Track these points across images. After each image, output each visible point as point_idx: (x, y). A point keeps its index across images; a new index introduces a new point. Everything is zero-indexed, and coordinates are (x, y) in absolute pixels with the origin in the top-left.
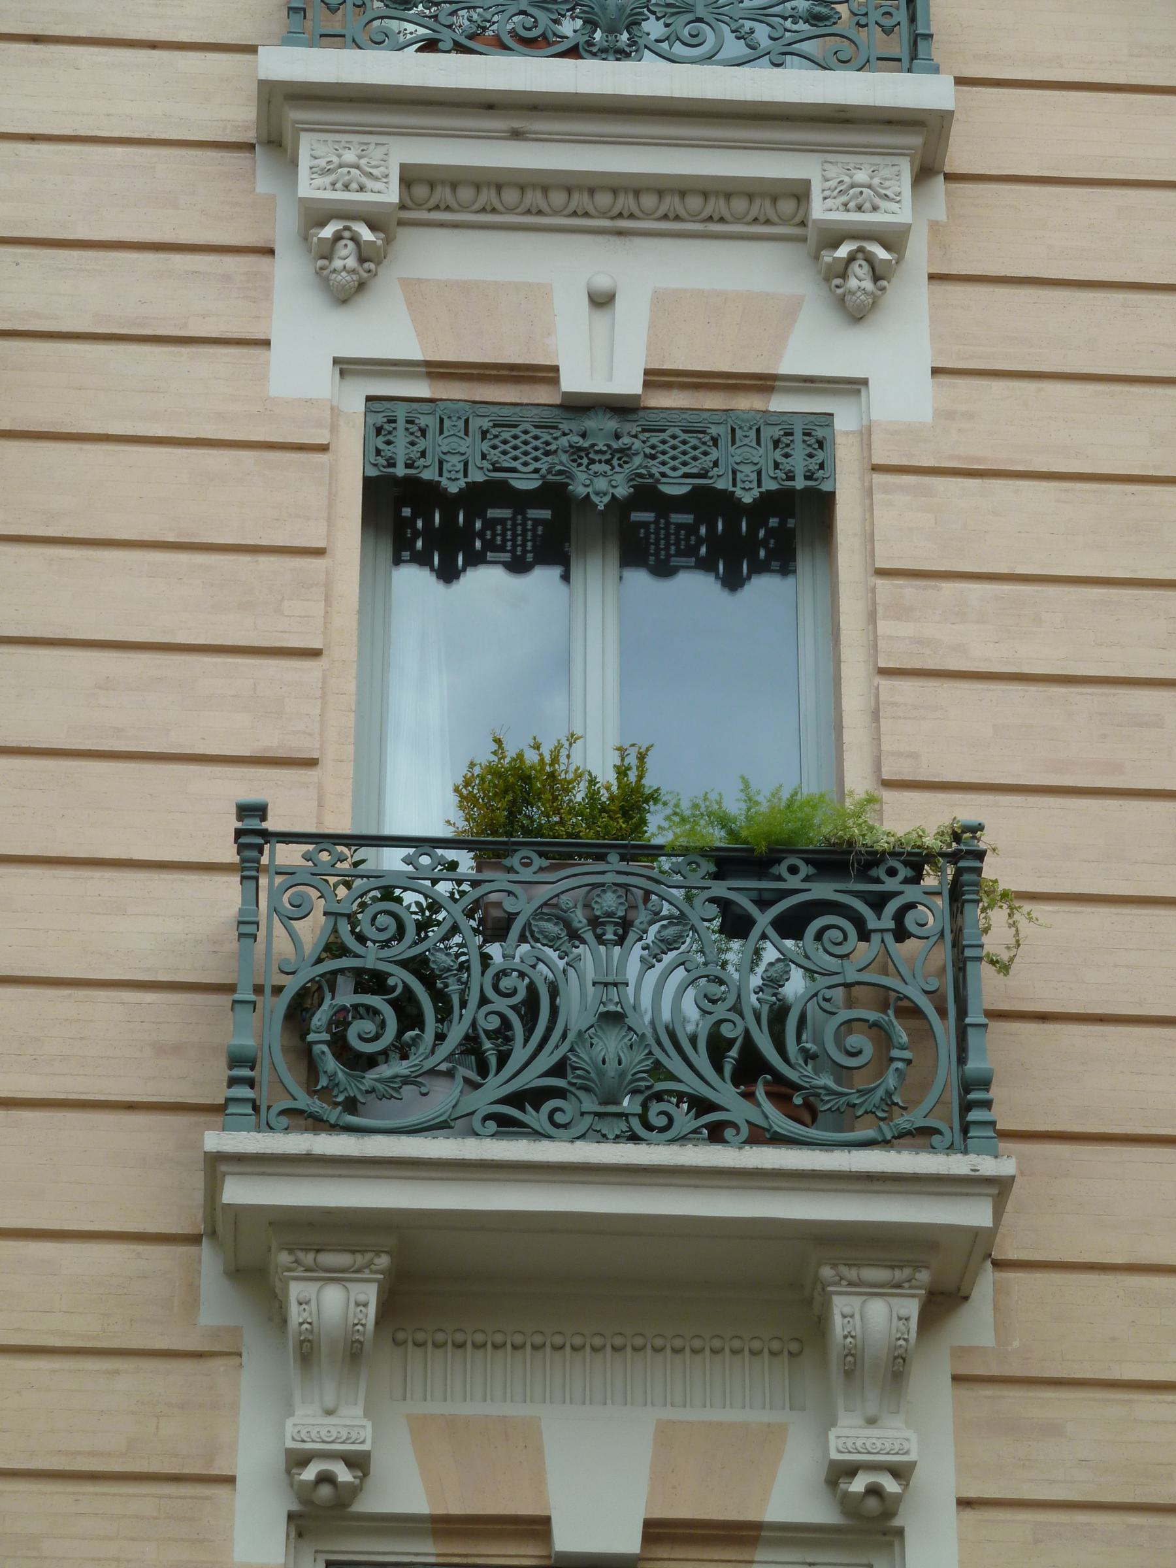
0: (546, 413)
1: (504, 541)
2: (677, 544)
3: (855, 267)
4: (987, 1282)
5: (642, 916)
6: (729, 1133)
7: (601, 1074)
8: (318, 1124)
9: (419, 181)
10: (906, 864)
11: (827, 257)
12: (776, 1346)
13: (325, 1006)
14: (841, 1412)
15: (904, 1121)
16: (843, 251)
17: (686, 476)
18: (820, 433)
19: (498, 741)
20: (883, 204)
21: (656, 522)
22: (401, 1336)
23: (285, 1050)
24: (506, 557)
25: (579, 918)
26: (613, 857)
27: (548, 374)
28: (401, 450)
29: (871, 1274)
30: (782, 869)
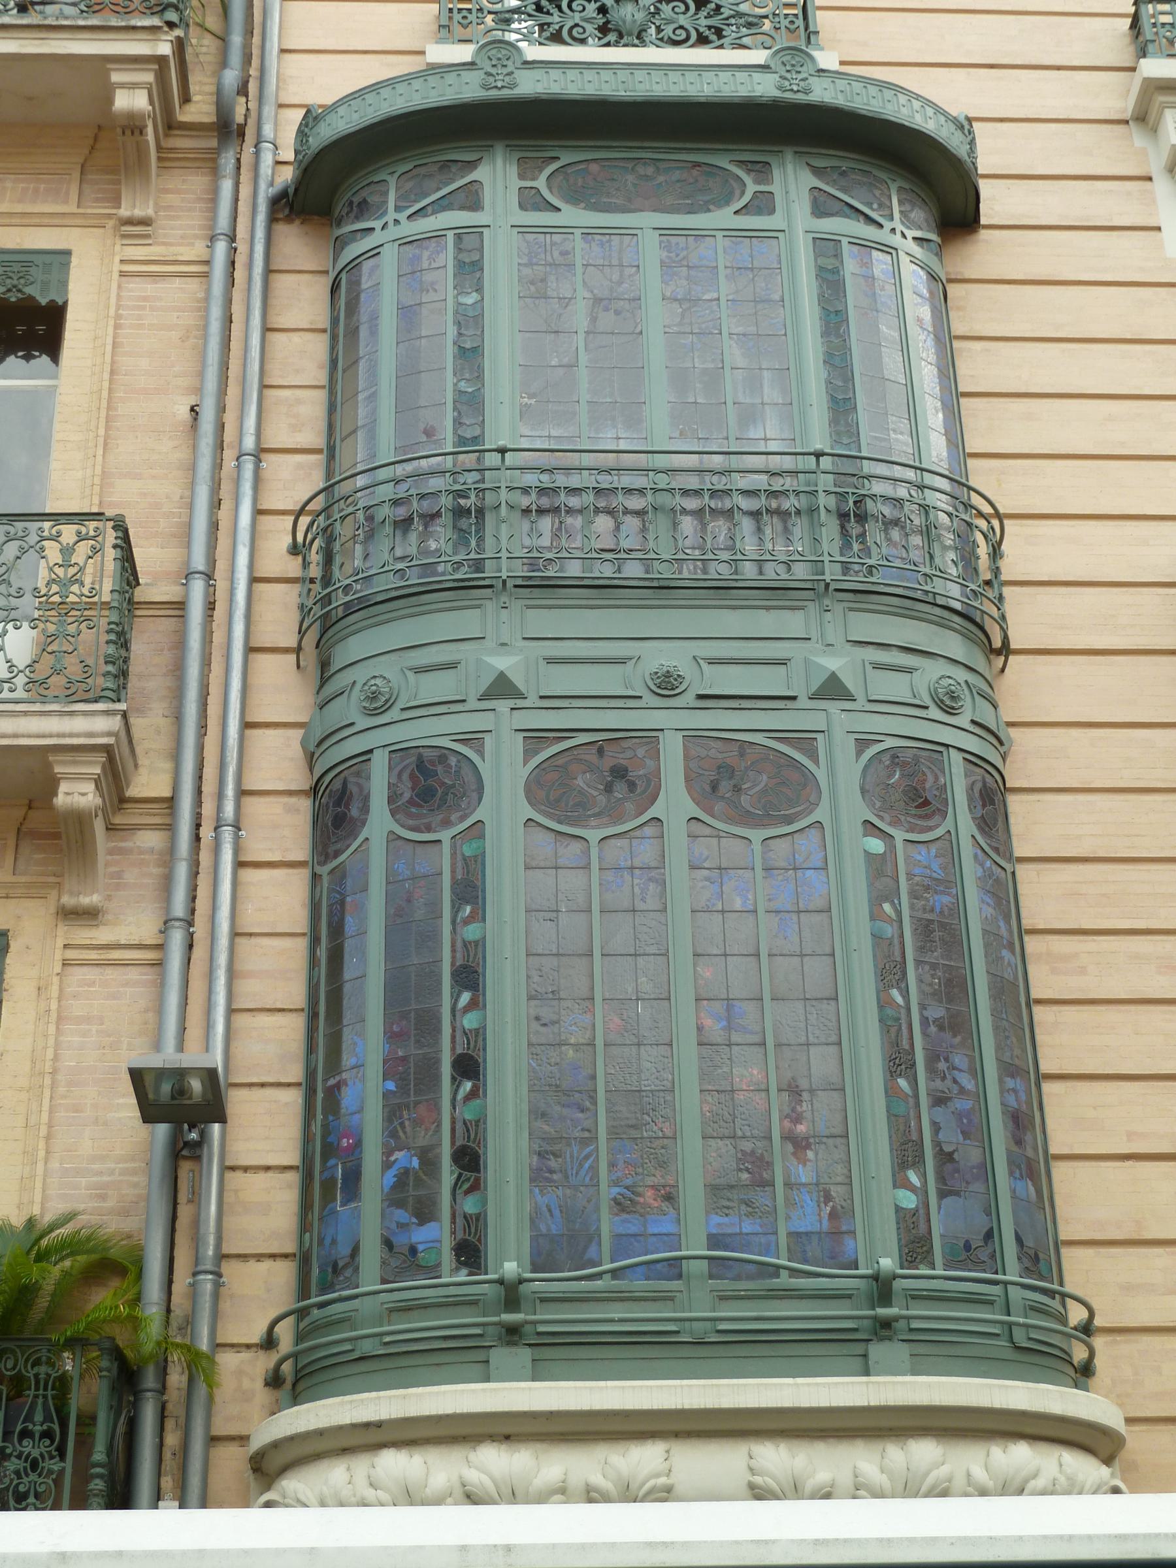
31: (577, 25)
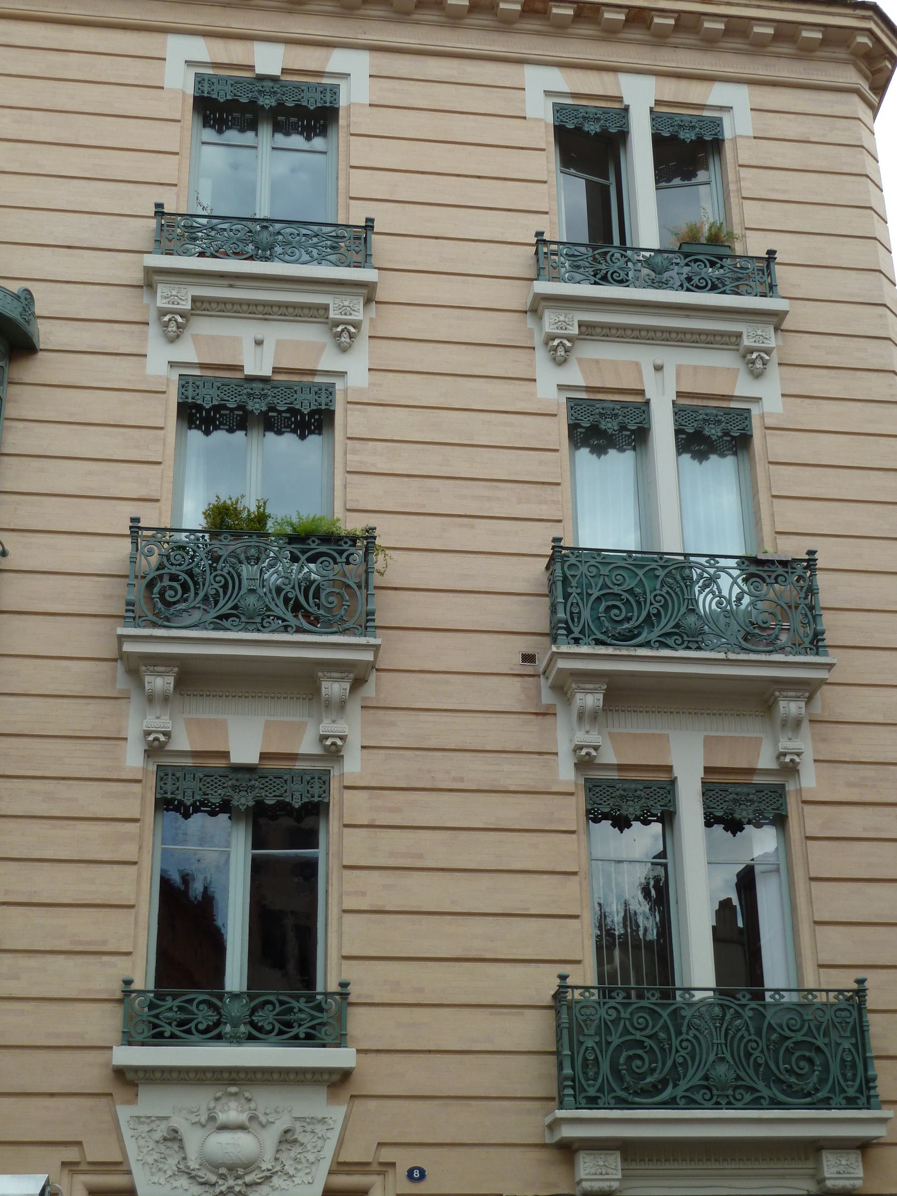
0: (239, 381)
1: (227, 422)
2: (284, 424)
3: (344, 333)
4: (373, 676)
5: (263, 557)
6: (289, 629)
7: (248, 609)
8: (155, 625)
9: (198, 301)
10: (350, 540)
11: (335, 330)
12: (304, 696)
13: (158, 586)
14: (324, 719)
15: (346, 626)
16: (339, 329)
17: (286, 403)
18: (330, 390)
19: (218, 497)
20: (353, 313)
21: (277, 416)
22: (183, 692)
23: (144, 597)
24: (227, 427)
25: (242, 557)
26: (254, 537)
27: (240, 368)
28: (190, 393)
29: (334, 675)
30: (310, 541)
31: (615, 272)
